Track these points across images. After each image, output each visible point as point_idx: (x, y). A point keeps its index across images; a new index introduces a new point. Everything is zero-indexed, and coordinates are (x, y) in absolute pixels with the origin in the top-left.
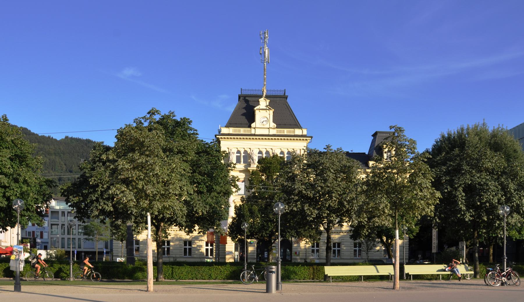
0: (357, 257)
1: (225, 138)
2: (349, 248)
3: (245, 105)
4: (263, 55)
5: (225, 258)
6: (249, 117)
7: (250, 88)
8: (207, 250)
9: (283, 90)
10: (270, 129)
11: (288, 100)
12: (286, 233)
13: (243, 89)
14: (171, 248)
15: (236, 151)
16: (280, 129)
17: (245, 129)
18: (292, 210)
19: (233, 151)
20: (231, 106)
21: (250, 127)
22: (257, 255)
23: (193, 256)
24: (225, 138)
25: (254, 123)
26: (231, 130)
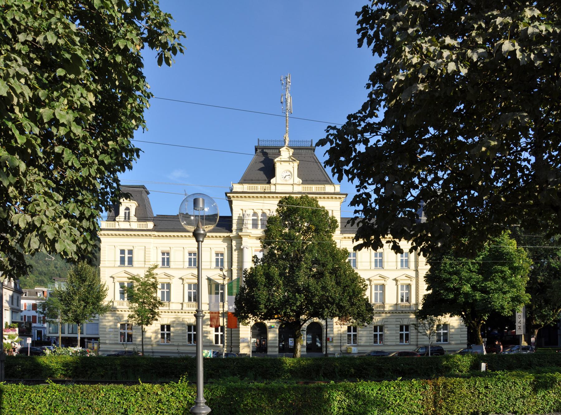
0: (404, 343)
1: (237, 197)
2: (394, 332)
3: (263, 158)
4: (284, 103)
5: (238, 347)
6: (269, 171)
7: (268, 138)
8: (217, 336)
9: (310, 140)
10: (294, 186)
11: (315, 153)
12: (324, 309)
13: (260, 139)
14: (172, 334)
15: (251, 213)
16: (307, 186)
17: (263, 186)
18: (497, 60)
19: (248, 212)
20: (248, 159)
21: (269, 183)
22: (280, 342)
23: (134, 342)
24: (237, 197)
25: (275, 178)
26: (246, 187)
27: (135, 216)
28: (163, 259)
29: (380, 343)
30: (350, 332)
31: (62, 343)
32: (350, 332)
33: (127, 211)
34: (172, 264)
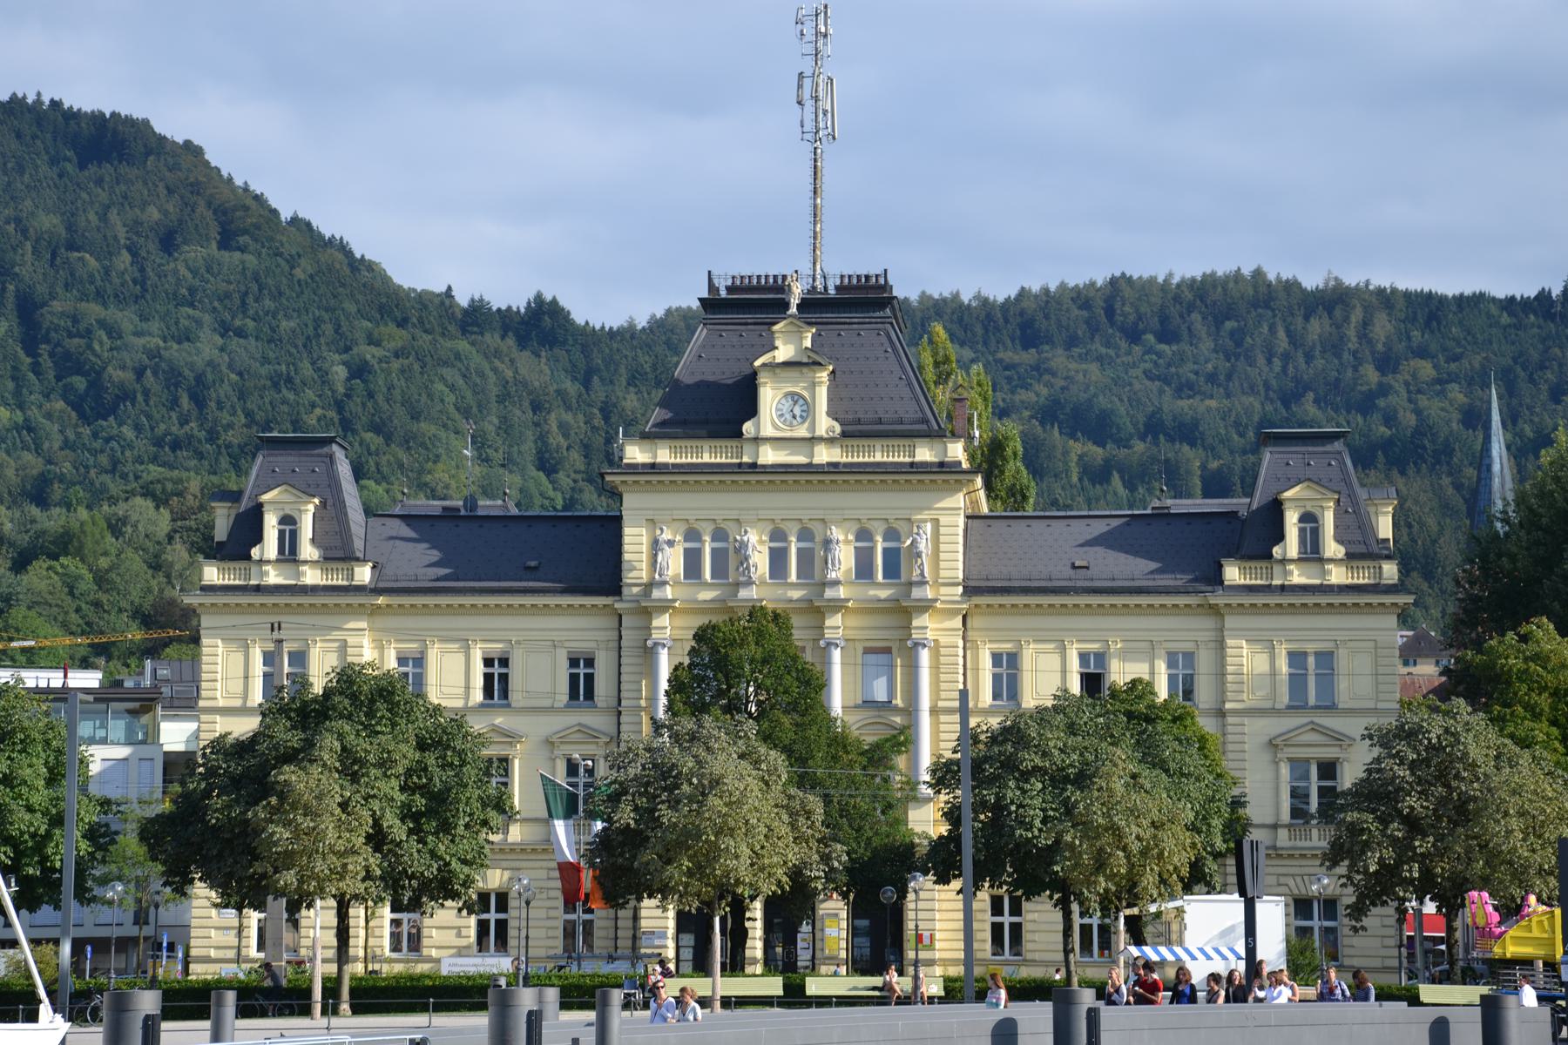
27: (313, 540)
28: (574, 679)
29: (1102, 955)
30: (1001, 914)
31: (307, 993)
32: (1001, 914)
33: (288, 528)
34: (516, 697)
